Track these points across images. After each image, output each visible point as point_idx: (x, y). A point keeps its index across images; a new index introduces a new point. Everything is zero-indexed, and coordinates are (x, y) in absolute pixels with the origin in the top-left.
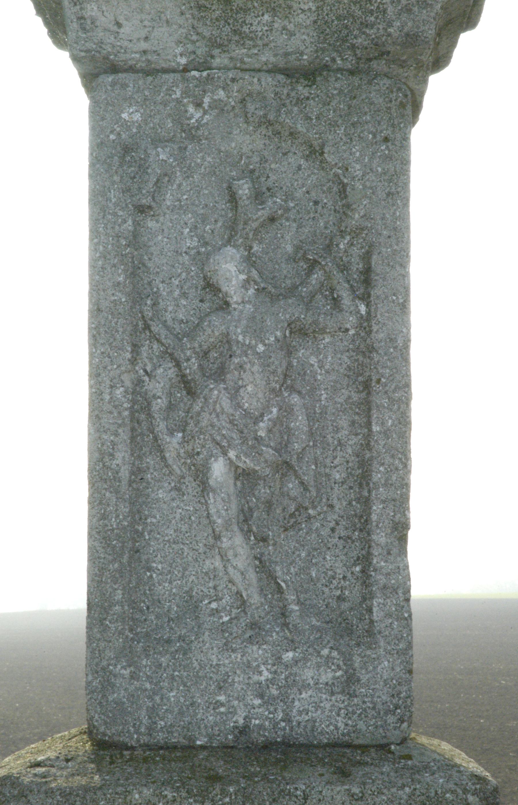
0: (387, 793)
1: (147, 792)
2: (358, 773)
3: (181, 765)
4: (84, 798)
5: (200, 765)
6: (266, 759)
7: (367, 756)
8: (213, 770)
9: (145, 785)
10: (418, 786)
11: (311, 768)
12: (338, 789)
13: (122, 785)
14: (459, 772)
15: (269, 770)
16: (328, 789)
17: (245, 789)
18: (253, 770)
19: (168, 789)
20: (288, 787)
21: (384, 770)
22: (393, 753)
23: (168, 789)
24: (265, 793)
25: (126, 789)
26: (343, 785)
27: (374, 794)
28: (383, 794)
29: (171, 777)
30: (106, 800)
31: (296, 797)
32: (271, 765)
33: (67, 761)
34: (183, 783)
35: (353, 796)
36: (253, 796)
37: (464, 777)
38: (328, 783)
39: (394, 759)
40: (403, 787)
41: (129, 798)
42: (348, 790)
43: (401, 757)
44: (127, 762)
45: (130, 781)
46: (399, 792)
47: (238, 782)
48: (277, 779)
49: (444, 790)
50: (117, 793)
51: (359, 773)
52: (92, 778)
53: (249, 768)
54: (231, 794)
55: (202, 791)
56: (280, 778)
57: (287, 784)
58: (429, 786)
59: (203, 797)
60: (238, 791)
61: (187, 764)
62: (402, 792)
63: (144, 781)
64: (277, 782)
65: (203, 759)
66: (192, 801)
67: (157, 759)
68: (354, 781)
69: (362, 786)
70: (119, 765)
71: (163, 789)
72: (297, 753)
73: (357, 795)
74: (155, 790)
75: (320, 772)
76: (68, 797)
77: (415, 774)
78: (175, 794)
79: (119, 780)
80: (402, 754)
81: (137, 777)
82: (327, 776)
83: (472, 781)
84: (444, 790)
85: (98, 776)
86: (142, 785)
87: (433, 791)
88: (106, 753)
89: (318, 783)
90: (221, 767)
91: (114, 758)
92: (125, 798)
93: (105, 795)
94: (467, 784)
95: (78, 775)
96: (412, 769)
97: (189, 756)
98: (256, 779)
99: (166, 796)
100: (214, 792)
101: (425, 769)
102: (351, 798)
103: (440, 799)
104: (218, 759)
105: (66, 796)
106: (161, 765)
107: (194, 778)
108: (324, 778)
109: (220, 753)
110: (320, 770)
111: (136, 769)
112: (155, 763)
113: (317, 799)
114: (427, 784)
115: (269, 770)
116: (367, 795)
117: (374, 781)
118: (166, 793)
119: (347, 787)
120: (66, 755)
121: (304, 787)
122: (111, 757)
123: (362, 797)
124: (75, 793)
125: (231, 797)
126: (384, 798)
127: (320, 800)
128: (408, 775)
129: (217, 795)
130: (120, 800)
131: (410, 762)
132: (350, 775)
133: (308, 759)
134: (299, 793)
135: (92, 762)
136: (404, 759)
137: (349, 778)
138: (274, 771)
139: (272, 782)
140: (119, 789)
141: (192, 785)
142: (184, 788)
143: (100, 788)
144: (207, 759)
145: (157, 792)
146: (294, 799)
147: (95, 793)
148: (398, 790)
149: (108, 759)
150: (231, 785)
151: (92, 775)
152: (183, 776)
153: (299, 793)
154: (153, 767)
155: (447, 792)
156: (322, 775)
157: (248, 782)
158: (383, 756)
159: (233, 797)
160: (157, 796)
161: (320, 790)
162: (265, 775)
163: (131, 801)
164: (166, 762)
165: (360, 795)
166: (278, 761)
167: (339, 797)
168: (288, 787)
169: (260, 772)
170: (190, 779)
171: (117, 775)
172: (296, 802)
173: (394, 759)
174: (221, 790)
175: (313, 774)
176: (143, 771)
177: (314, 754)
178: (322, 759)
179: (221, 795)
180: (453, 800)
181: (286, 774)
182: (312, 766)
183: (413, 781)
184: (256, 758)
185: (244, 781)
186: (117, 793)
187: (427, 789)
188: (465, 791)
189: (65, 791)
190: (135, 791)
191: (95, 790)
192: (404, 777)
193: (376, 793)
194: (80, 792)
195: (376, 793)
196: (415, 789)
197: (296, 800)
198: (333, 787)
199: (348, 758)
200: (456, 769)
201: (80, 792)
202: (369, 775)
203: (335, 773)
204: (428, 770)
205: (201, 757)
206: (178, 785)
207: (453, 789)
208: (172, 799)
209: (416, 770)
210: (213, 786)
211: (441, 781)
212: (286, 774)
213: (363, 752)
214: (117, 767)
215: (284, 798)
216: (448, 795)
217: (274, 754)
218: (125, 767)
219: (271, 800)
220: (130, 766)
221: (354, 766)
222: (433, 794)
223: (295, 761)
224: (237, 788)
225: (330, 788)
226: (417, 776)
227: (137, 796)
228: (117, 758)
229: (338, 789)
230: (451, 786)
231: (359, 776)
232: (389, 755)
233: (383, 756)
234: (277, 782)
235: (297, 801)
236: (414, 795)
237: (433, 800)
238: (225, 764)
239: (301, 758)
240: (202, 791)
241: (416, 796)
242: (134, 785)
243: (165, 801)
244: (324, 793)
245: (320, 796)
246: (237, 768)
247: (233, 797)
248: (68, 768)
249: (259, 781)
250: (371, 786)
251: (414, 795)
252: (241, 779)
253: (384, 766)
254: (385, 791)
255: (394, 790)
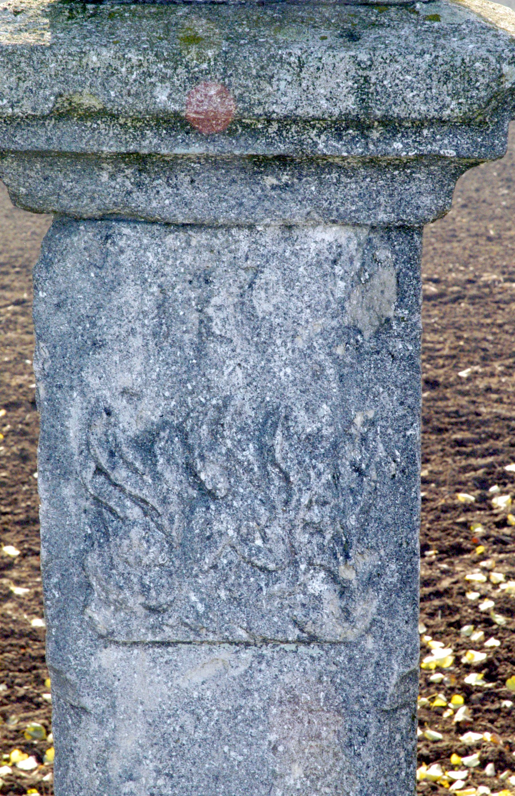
0: (402, 61)
1: (107, 54)
2: (369, 37)
3: (153, 22)
4: (30, 58)
5: (176, 24)
6: (258, 18)
7: (385, 16)
8: (191, 29)
9: (105, 46)
10: (441, 53)
11: (313, 30)
12: (342, 55)
13: (77, 45)
14: (496, 36)
15: (260, 31)
16: (329, 55)
17: (226, 53)
18: (240, 30)
19: (133, 50)
20: (280, 52)
21: (403, 33)
22: (418, 13)
23: (133, 50)
24: (251, 59)
25: (81, 49)
26: (347, 51)
27: (386, 63)
28: (396, 62)
29: (139, 37)
30: (57, 61)
31: (289, 64)
32: (264, 25)
33: (16, 13)
34: (152, 45)
35: (359, 65)
36: (236, 63)
37: (501, 42)
38: (330, 47)
39: (418, 20)
40: (423, 53)
41: (84, 61)
42: (353, 57)
43: (426, 18)
44: (89, 17)
45: (88, 40)
46: (417, 60)
47: (219, 45)
48: (267, 42)
49: (473, 58)
50: (70, 54)
51: (369, 37)
52: (43, 34)
53: (237, 28)
54: (209, 59)
55: (174, 54)
56: (272, 41)
57: (279, 48)
58: (454, 52)
59: (176, 62)
60: (218, 55)
61: (161, 22)
62: (421, 60)
63: (104, 41)
64: (267, 46)
65: (181, 16)
66: (162, 66)
67: (127, 15)
68: (362, 46)
69: (372, 53)
70: (78, 20)
71: (126, 51)
72: (299, 11)
73: (364, 63)
74: (116, 52)
75: (322, 35)
76: (11, 57)
77: (440, 38)
78: (141, 58)
79: (74, 38)
80: (428, 14)
81: (97, 36)
82: (329, 40)
83: (510, 48)
84: (473, 58)
85: (49, 33)
86: (101, 45)
87: (459, 59)
88: (65, 5)
89: (317, 48)
90: (202, 26)
91: (74, 12)
92: (80, 60)
93: (55, 55)
94: (503, 50)
95: (26, 31)
96: (437, 32)
97: (165, 13)
98: (242, 42)
99: (130, 60)
100: (189, 56)
101: (454, 32)
102: (357, 67)
103: (468, 69)
104: (200, 17)
105: (9, 55)
106: (129, 22)
107: (166, 39)
108: (326, 42)
109: (204, 9)
110: (323, 32)
111: (97, 26)
112: (123, 18)
113: (315, 67)
114: (453, 51)
115: (260, 31)
116: (376, 63)
117: (386, 46)
118: (129, 55)
119: (352, 53)
120: (16, 7)
121: (299, 53)
122: (71, 10)
123: (370, 66)
124: (19, 52)
125: (209, 63)
126: (398, 67)
127: (318, 69)
128: (431, 39)
129: (193, 60)
130: (74, 62)
131: (436, 24)
132: (359, 39)
133: (311, 19)
134: (292, 59)
135: (47, 16)
136: (430, 20)
137: (357, 43)
138: (267, 32)
139: (261, 45)
140: (74, 49)
141: (162, 47)
142: (152, 50)
143: (50, 47)
144: (186, 16)
145: (120, 54)
146: (286, 66)
147: (43, 53)
148: (416, 58)
149: (67, 14)
150: (211, 48)
151: (43, 32)
152: (154, 36)
153: (292, 59)
154: (118, 25)
155: (476, 60)
156: (324, 38)
157: (232, 45)
158: (404, 17)
159: (212, 63)
160: (119, 59)
161: (320, 56)
162: (255, 36)
163: (87, 65)
164: (137, 18)
165: (369, 63)
166: (274, 20)
167: (342, 65)
168: (280, 52)
169: (248, 33)
170: (162, 39)
171: (74, 32)
172: (289, 71)
173: (418, 20)
174: (197, 54)
175: (313, 37)
176: (106, 28)
177: (320, 13)
178: (328, 19)
179: (197, 59)
180: (483, 70)
181: (280, 37)
182: (314, 27)
183: (435, 46)
184: (247, 17)
185: (227, 43)
186: (70, 54)
187: (452, 56)
188: (500, 59)
189: (7, 49)
190: (92, 52)
191: (43, 49)
192: (425, 41)
193: (388, 61)
194: (25, 51)
195: (388, 61)
196: (437, 57)
197: (289, 68)
198: (335, 53)
199: (361, 19)
200: (492, 32)
201: (25, 51)
202: (382, 39)
203: (342, 36)
204: (457, 33)
205: (180, 13)
206: (145, 46)
207: (484, 57)
208: (137, 63)
209: (442, 34)
210: (187, 49)
211: (471, 46)
212: (280, 37)
213: (380, 12)
214: (75, 23)
215: (274, 65)
216: (477, 64)
217: (269, 12)
218: (85, 23)
219: (258, 67)
220: (91, 22)
221: (365, 28)
222: (458, 63)
223: (295, 21)
224: (217, 53)
225: (331, 54)
226: (442, 41)
227: (95, 59)
228: (78, 12)
229: (342, 55)
230: (483, 53)
231: (370, 40)
232: (412, 16)
233: (404, 17)
234: (267, 46)
235: (291, 69)
236: (435, 64)
237: (459, 70)
238: (207, 23)
239: (302, 17)
240: (174, 54)
241: (438, 65)
242: (92, 44)
243: (128, 65)
244: (324, 60)
245: (319, 64)
246: (221, 28)
247: (212, 63)
248: (16, 22)
249: (245, 44)
250: (382, 52)
251: (435, 64)
252: (224, 41)
253: (403, 28)
254: (400, 58)
255: (411, 57)
